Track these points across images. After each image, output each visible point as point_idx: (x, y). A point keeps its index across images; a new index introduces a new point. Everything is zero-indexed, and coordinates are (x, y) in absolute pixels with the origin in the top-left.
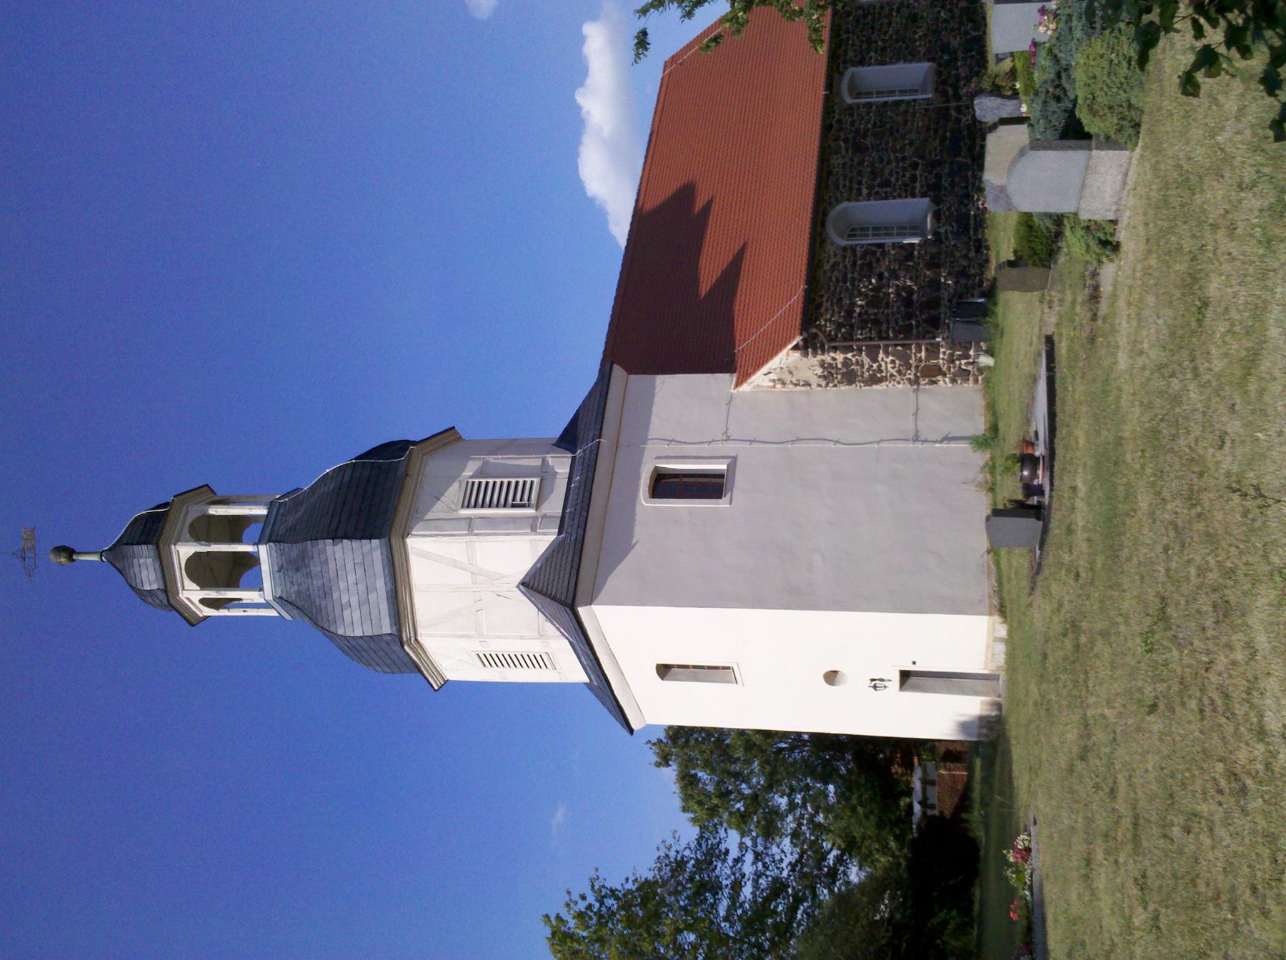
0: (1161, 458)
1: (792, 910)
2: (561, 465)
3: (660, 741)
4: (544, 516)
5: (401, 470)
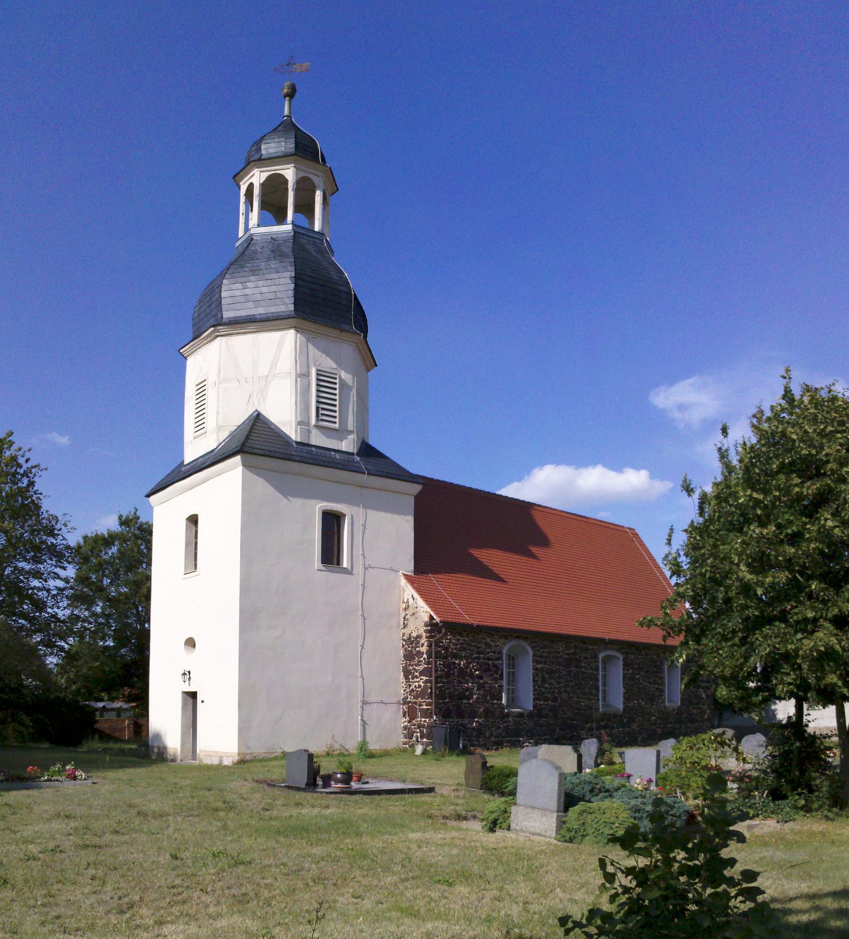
0: (346, 860)
1: (24, 616)
2: (348, 445)
3: (138, 518)
4: (309, 431)
5: (346, 327)
